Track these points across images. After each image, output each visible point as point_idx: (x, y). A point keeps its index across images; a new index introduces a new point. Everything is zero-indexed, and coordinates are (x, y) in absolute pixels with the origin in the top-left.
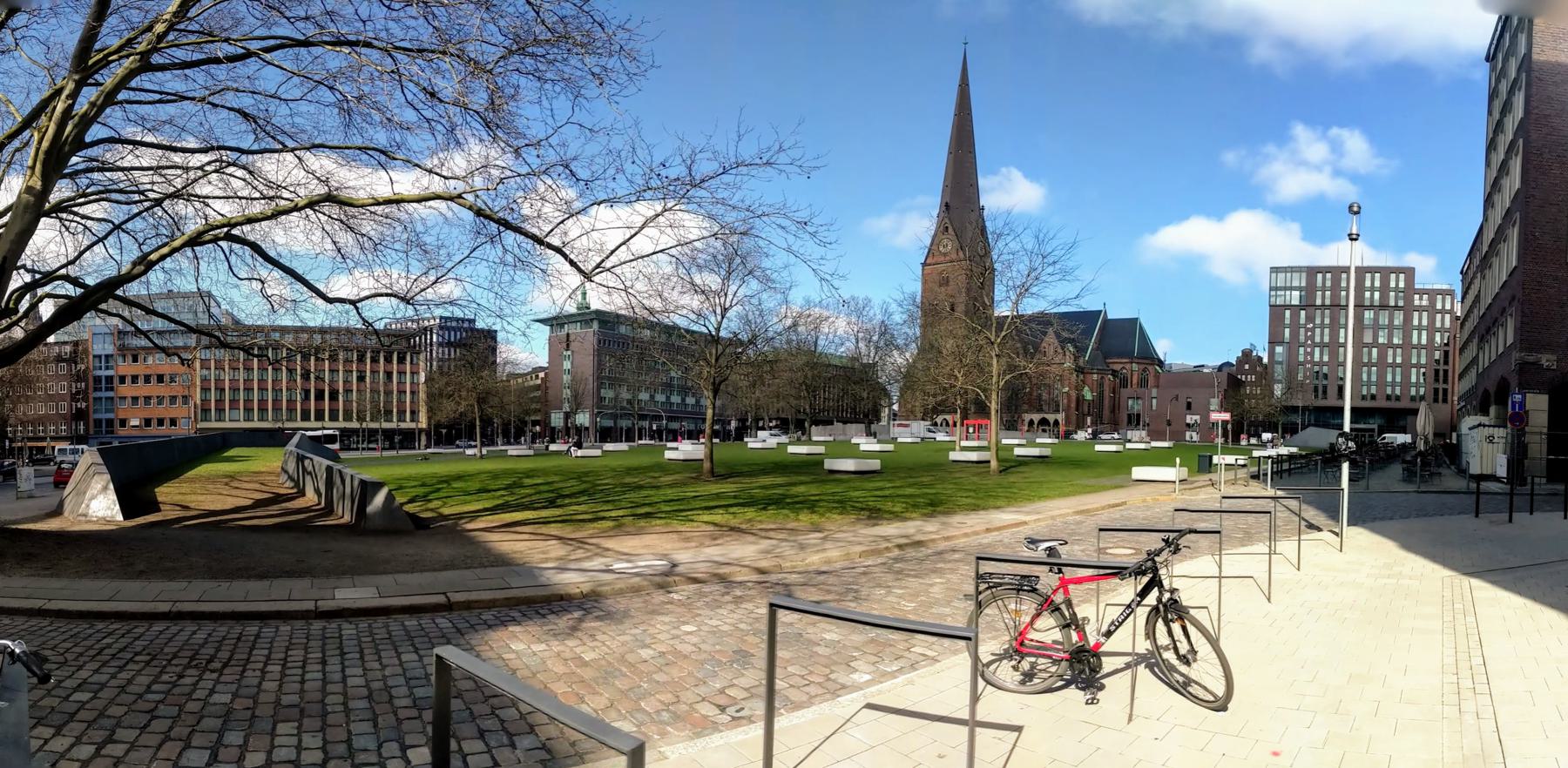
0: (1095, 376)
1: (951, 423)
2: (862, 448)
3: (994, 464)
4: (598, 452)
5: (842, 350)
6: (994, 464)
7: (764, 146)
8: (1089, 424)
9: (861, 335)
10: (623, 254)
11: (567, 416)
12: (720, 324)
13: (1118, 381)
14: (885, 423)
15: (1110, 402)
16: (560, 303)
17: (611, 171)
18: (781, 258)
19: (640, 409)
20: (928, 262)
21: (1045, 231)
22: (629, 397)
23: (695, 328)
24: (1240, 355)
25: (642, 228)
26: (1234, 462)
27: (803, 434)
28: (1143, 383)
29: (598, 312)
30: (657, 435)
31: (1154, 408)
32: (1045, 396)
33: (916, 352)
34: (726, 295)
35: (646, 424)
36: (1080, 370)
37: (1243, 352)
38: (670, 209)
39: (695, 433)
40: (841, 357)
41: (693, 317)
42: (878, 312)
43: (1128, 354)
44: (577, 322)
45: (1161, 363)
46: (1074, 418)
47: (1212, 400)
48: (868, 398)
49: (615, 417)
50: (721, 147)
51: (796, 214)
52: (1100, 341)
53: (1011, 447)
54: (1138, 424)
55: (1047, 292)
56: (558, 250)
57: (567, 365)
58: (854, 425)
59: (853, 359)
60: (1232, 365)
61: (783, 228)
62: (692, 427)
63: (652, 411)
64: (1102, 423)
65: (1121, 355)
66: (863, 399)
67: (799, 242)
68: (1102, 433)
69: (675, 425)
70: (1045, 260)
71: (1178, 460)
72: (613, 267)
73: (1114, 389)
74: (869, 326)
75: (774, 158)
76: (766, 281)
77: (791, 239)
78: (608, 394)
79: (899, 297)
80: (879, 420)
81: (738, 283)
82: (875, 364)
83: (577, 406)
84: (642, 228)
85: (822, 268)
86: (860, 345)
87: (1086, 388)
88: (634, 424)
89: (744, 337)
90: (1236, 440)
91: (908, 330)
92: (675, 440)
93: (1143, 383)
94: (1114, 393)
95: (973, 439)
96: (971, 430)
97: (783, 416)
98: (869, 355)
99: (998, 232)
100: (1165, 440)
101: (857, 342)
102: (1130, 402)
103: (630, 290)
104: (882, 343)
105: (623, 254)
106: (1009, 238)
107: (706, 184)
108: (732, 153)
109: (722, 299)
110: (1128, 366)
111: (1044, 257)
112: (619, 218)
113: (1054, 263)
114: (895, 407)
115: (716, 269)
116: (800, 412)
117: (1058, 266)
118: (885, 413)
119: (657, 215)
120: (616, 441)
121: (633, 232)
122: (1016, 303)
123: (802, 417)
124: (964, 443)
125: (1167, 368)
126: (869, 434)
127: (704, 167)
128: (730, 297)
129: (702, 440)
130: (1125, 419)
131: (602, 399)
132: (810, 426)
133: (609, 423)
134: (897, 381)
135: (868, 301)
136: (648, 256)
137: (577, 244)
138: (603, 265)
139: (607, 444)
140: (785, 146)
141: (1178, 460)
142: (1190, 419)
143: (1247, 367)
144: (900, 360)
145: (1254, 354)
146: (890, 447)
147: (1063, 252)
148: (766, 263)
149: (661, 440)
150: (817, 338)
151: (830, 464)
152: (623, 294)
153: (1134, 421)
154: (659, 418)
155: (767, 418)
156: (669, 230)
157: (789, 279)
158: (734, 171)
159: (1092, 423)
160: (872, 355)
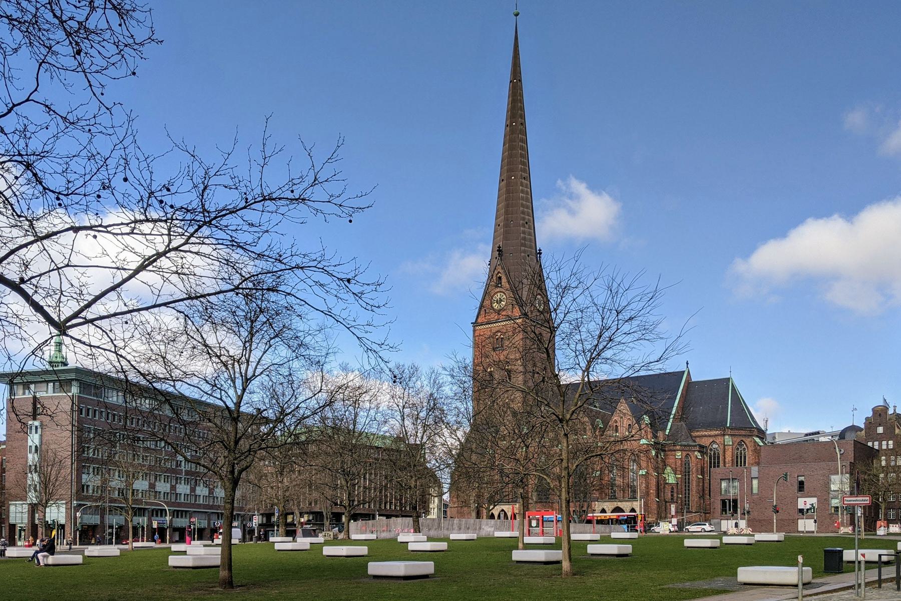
0: (679, 453)
1: (509, 514)
2: (411, 547)
3: (566, 565)
4: (78, 559)
5: (386, 428)
6: (566, 565)
7: (295, 175)
8: (673, 513)
9: (407, 411)
10: (110, 304)
11: (33, 508)
12: (240, 398)
13: (707, 459)
14: (435, 516)
15: (698, 485)
16: (19, 359)
17: (95, 185)
18: (315, 319)
19: (135, 501)
20: (479, 321)
21: (618, 280)
22: (123, 486)
23: (211, 400)
24: (870, 414)
25: (137, 271)
26: (876, 559)
27: (340, 531)
28: (739, 460)
29: (77, 370)
30: (160, 534)
31: (755, 491)
32: (619, 481)
33: (468, 429)
34: (248, 361)
35: (143, 521)
36: (660, 447)
37: (874, 410)
38: (176, 249)
39: (208, 532)
40: (384, 437)
41: (207, 388)
42: (425, 383)
43: (720, 425)
44: (47, 382)
45: (762, 434)
46: (654, 506)
47: (833, 477)
48: (416, 486)
49: (102, 512)
50: (242, 172)
51: (337, 269)
52: (683, 407)
53: (585, 543)
54: (735, 511)
55: (623, 355)
56: (16, 287)
57: (34, 439)
58: (400, 520)
59: (399, 439)
60: (860, 429)
61: (321, 285)
62: (204, 524)
63: (152, 504)
64: (689, 512)
65: (710, 426)
66: (410, 488)
67: (342, 305)
68: (689, 523)
69: (181, 522)
70: (620, 317)
71: (800, 559)
72: (102, 318)
73: (703, 468)
74: (415, 400)
75: (309, 191)
76: (298, 346)
77: (331, 301)
78: (91, 480)
79: (450, 363)
80: (427, 512)
81: (262, 347)
82: (422, 445)
83: (47, 495)
84: (137, 271)
85: (367, 336)
86: (407, 422)
87: (668, 469)
88: (126, 520)
89: (270, 414)
90: (871, 526)
91: (459, 404)
92: (182, 540)
93: (739, 460)
94: (703, 473)
95: (537, 535)
96: (534, 523)
97: (317, 510)
98: (416, 435)
99: (563, 284)
100: (771, 531)
101: (403, 420)
102: (724, 484)
103: (121, 352)
104: (431, 421)
105: (110, 304)
106: (578, 292)
107: (224, 222)
108: (255, 183)
109: (244, 367)
110: (719, 440)
111: (618, 313)
112: (105, 253)
113: (631, 319)
114: (446, 497)
115: (236, 329)
116: (336, 504)
117: (635, 323)
118: (434, 504)
119: (159, 255)
120: (100, 542)
121: (126, 275)
122: (587, 370)
123: (337, 510)
124: (527, 540)
125: (769, 439)
126: (417, 530)
127: (218, 199)
128: (252, 365)
129: (217, 541)
130: (719, 506)
131: (82, 487)
132: (349, 521)
133: (95, 520)
134: (448, 466)
135: (415, 370)
136: (147, 309)
137: (44, 282)
138: (83, 314)
139: (90, 548)
140: (322, 177)
141: (800, 559)
142: (804, 503)
143: (880, 430)
144: (450, 441)
145: (891, 411)
146: (443, 546)
147: (641, 304)
148: (298, 324)
149: (163, 540)
150: (356, 415)
151: (375, 568)
152: (113, 357)
153: (730, 507)
154: (162, 512)
155: (297, 512)
156: (174, 278)
157: (325, 344)
158: (258, 206)
159: (677, 512)
160: (419, 435)
